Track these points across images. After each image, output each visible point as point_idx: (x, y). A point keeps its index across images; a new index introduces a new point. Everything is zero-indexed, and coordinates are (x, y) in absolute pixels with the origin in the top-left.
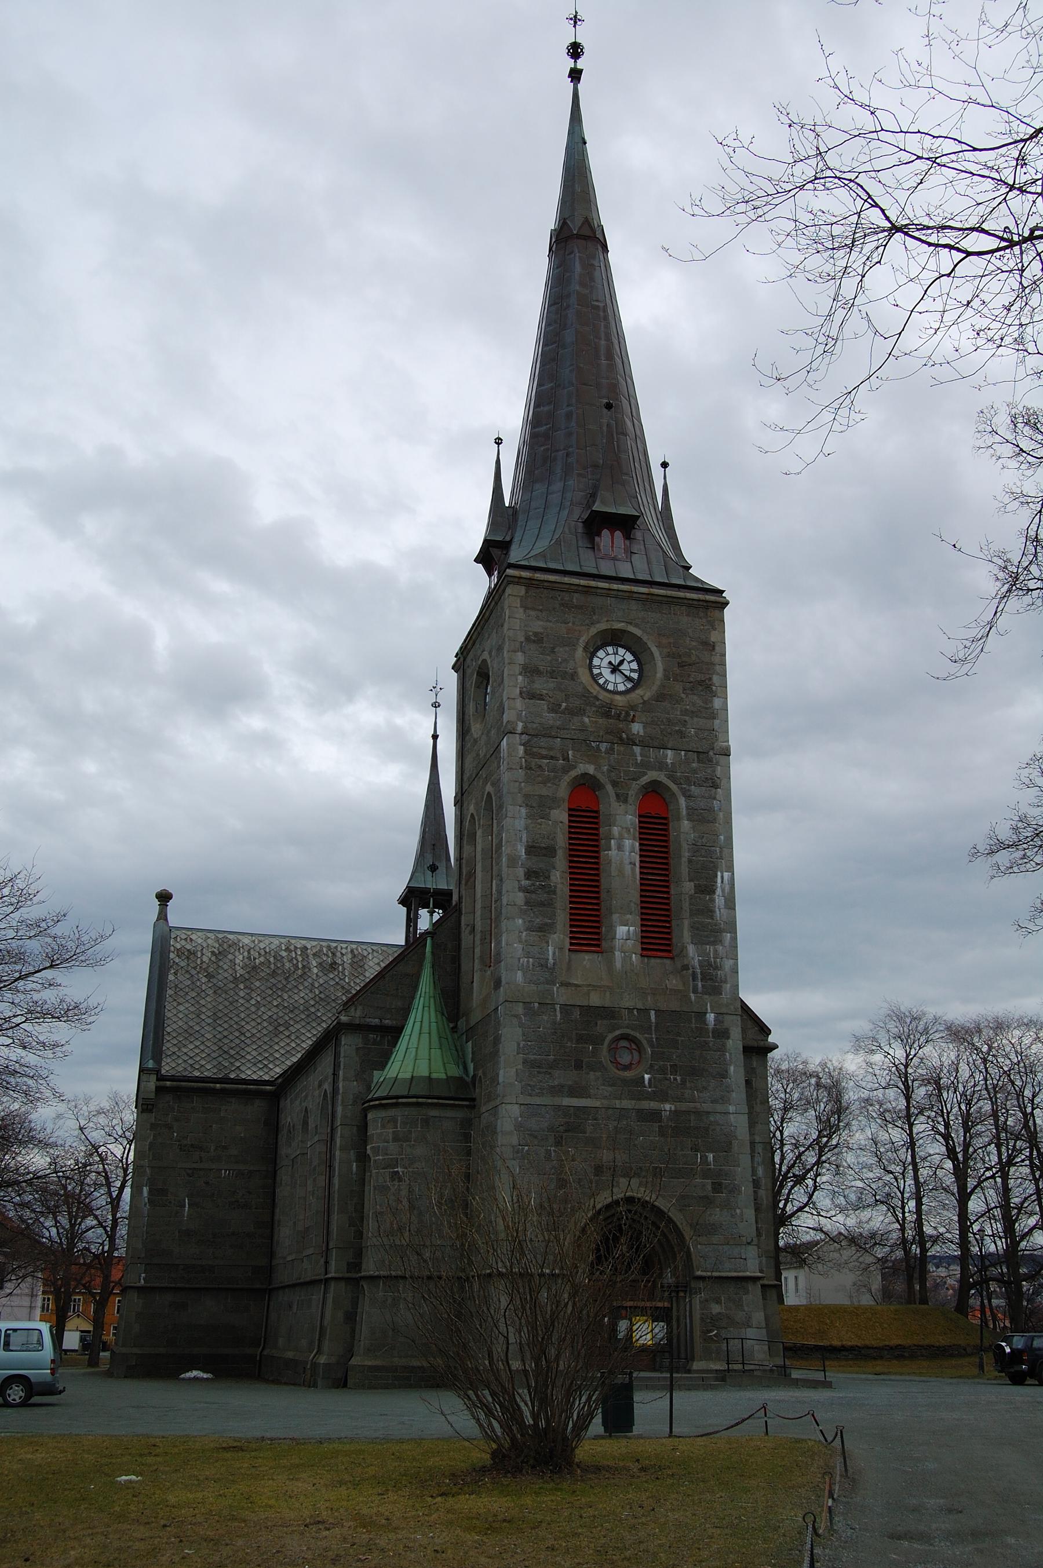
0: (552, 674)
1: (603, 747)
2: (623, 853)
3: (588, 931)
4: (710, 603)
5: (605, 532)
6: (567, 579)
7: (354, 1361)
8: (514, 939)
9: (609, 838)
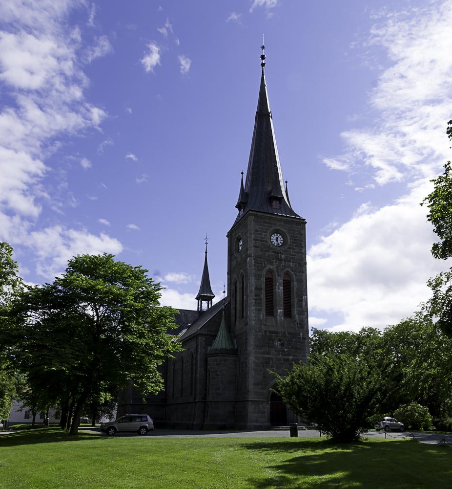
0: (261, 241)
1: (275, 261)
2: (279, 290)
3: (270, 311)
4: (302, 222)
5: (274, 202)
6: (265, 215)
7: (205, 423)
8: (252, 313)
9: (276, 285)
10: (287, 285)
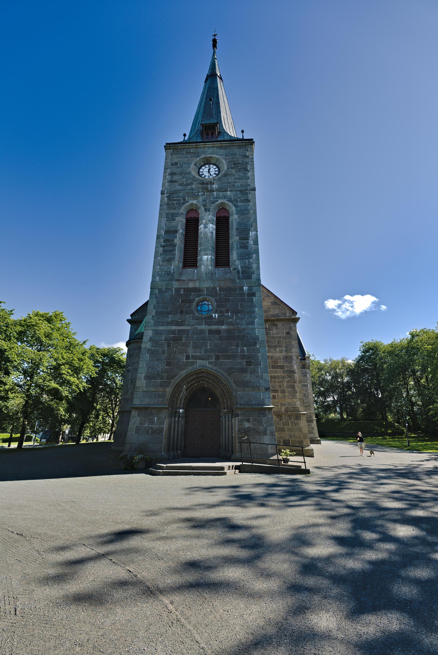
2: (208, 229)
10: (222, 223)
